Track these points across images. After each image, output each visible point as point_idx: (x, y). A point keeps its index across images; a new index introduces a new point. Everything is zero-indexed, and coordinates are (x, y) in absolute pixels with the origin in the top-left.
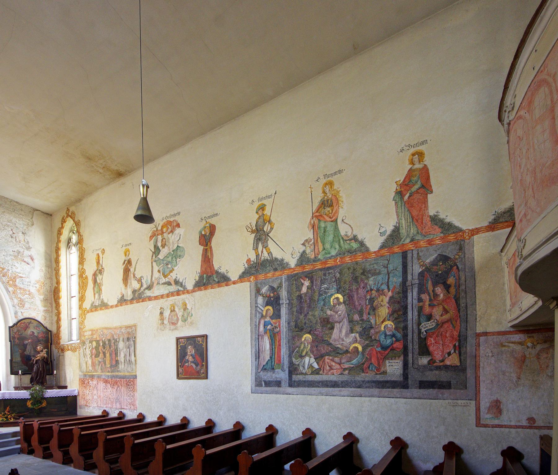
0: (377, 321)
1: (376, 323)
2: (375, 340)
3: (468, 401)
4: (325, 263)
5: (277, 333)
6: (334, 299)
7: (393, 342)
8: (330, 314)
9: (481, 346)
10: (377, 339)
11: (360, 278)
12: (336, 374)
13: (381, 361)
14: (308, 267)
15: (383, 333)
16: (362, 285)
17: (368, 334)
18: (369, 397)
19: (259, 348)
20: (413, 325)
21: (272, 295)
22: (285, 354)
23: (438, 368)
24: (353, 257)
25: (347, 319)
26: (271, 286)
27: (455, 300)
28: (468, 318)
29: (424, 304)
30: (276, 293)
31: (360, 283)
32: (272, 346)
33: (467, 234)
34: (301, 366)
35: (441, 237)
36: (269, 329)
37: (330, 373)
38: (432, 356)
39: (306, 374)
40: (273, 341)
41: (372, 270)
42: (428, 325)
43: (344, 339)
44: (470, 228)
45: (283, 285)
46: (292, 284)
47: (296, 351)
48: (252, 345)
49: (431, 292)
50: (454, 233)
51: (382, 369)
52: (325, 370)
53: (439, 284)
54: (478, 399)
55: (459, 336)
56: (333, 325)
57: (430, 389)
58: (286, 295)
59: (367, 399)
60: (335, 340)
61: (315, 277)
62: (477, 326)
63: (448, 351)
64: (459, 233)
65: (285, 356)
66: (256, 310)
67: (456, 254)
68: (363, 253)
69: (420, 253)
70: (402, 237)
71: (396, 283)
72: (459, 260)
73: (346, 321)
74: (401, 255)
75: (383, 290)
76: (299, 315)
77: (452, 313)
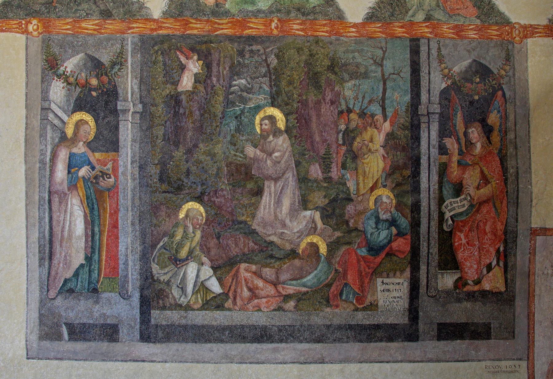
0: (361, 185)
1: (358, 189)
2: (356, 229)
3: (517, 363)
4: (243, 24)
5: (109, 190)
6: (262, 120)
7: (391, 237)
8: (252, 156)
9: (537, 254)
10: (360, 227)
11: (324, 77)
12: (265, 310)
13: (367, 280)
14: (198, 26)
15: (372, 215)
16: (329, 96)
17: (342, 215)
18: (341, 362)
19: (51, 228)
20: (429, 202)
21: (94, 82)
22: (129, 251)
23: (471, 296)
24: (308, 25)
25: (295, 173)
26: (92, 59)
27: (500, 159)
28: (520, 198)
29: (450, 160)
30: (105, 79)
31: (325, 89)
32: (93, 226)
33: (517, 32)
34: (174, 287)
35: (477, 26)
36: (83, 177)
37: (250, 306)
38: (461, 272)
39: (188, 308)
40: (96, 213)
41: (349, 64)
42: (456, 205)
43: (288, 221)
44: (522, 23)
45: (126, 61)
46: (155, 63)
47: (161, 244)
48: (31, 220)
49: (461, 135)
50: (497, 23)
51: (369, 299)
52: (238, 298)
53: (474, 121)
54: (531, 358)
55: (505, 233)
56: (262, 185)
57: (457, 340)
58: (137, 90)
59: (337, 367)
60: (265, 224)
61: (215, 56)
62: (533, 214)
63: (488, 261)
64: (506, 26)
65: (130, 258)
66: (44, 119)
67: (501, 67)
68: (330, 20)
69: (442, 49)
70: (409, 5)
71: (398, 103)
72: (506, 79)
73: (291, 177)
74: (408, 43)
75: (373, 116)
76: (172, 148)
77: (494, 186)
